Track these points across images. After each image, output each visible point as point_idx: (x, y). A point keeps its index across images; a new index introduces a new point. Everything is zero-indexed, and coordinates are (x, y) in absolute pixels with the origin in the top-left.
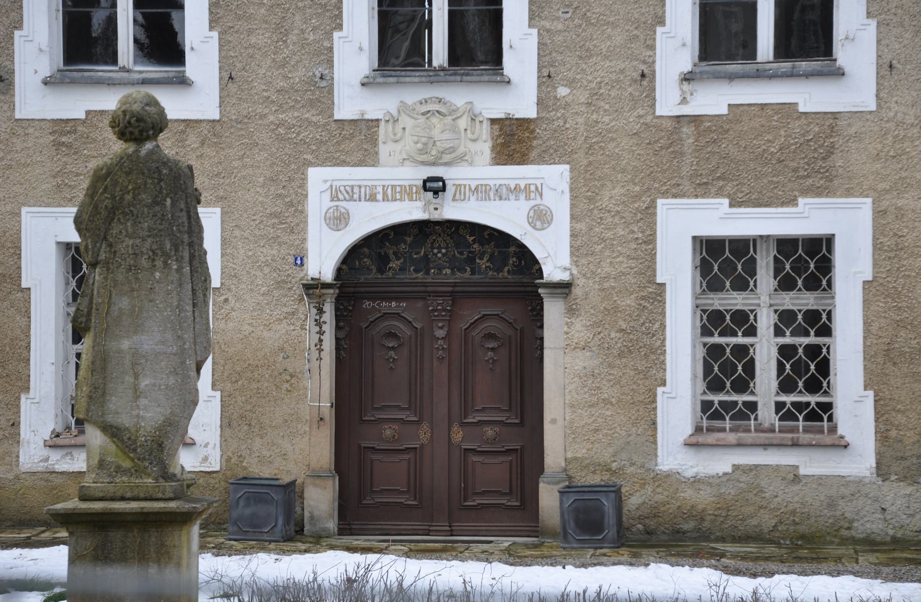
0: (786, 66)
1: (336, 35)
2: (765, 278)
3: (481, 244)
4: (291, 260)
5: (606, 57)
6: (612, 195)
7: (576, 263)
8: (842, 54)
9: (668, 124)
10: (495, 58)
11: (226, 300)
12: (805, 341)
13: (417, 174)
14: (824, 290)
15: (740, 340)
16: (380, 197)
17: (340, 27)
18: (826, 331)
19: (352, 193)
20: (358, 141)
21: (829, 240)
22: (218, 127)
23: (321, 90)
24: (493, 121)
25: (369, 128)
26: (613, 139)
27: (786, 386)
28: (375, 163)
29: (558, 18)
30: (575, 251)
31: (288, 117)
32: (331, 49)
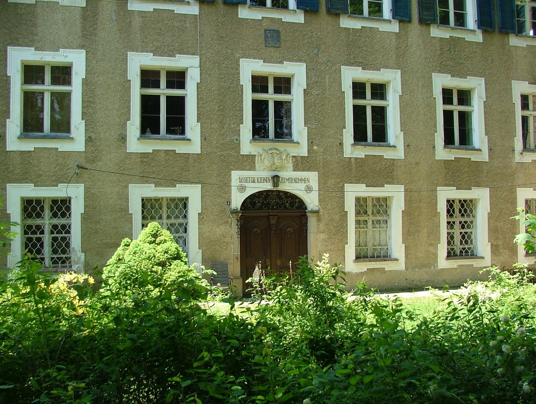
0: (374, 143)
1: (241, 125)
2: (47, 213)
3: (287, 198)
4: (226, 203)
5: (328, 138)
6: (331, 182)
7: (320, 204)
8: (189, 133)
9: (348, 160)
10: (68, 130)
11: (203, 217)
12: (36, 236)
13: (268, 174)
14: (68, 217)
15: (38, 235)
16: (256, 181)
17: (242, 123)
18: (69, 232)
19: (246, 180)
20: (249, 162)
21: (187, 199)
22: (200, 156)
23: (237, 145)
24: (293, 157)
25: (252, 158)
26: (331, 164)
27: (55, 251)
28: (254, 170)
29: (313, 124)
30: (320, 201)
31: (225, 153)
32: (239, 131)
